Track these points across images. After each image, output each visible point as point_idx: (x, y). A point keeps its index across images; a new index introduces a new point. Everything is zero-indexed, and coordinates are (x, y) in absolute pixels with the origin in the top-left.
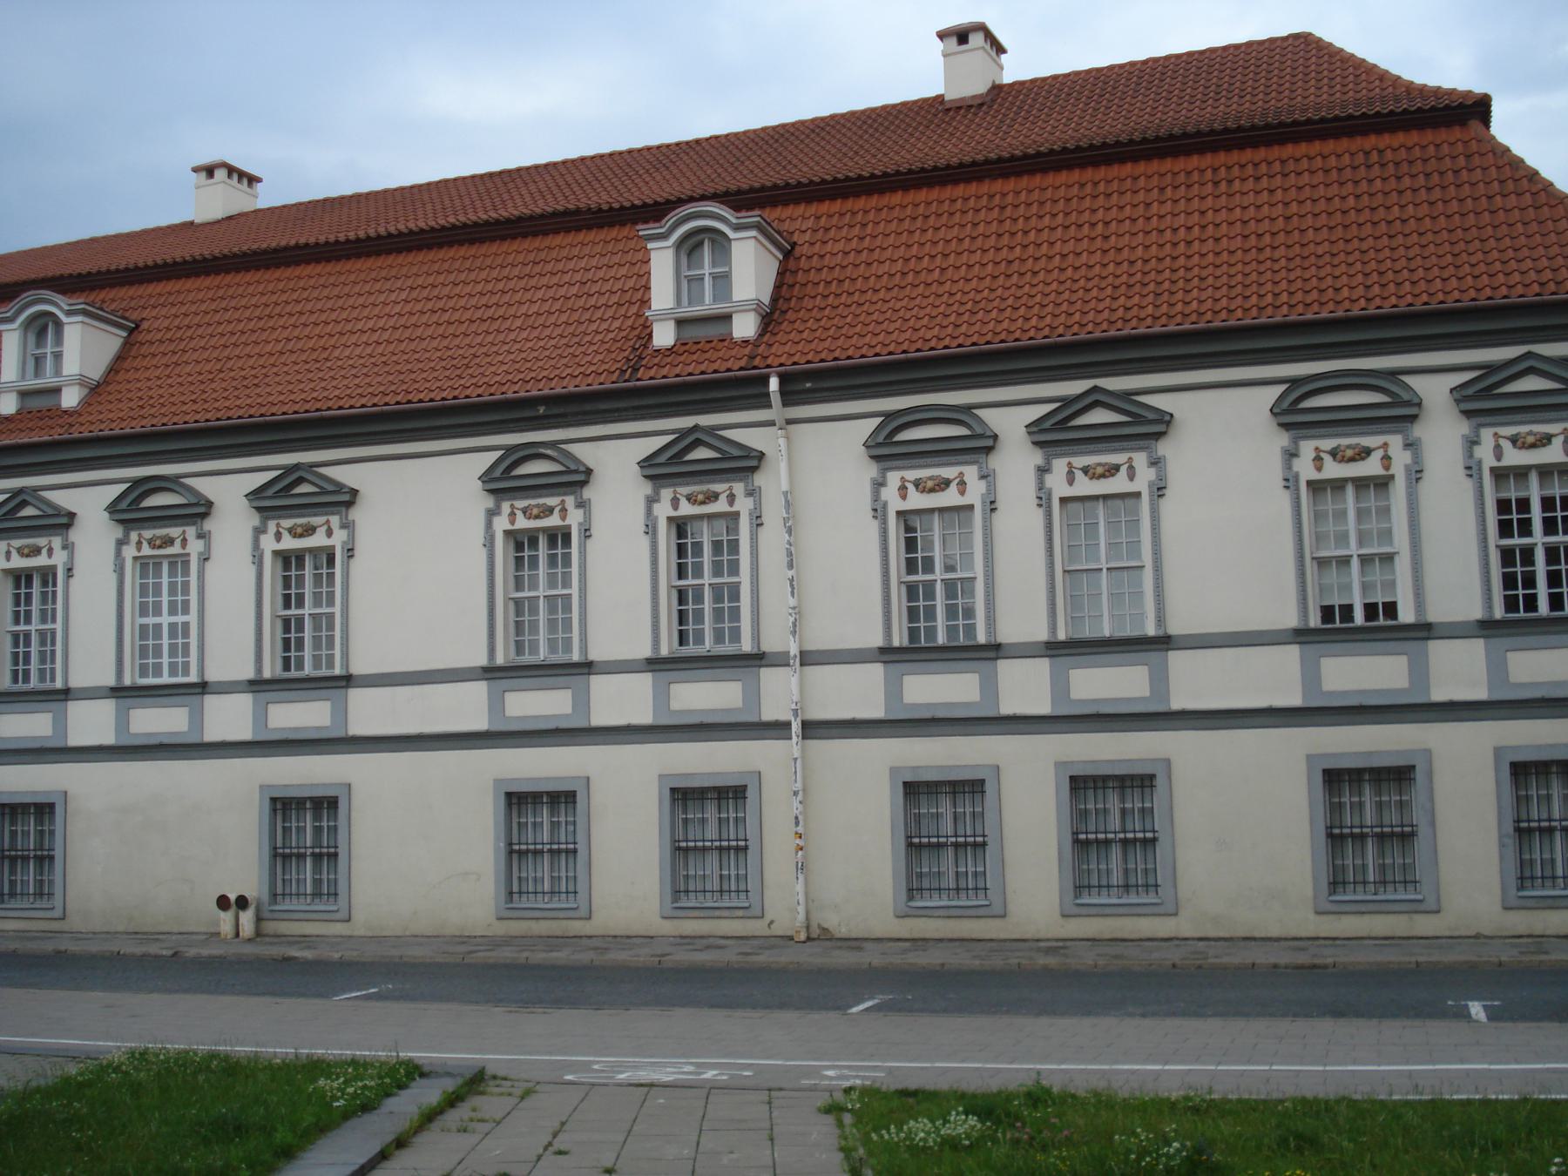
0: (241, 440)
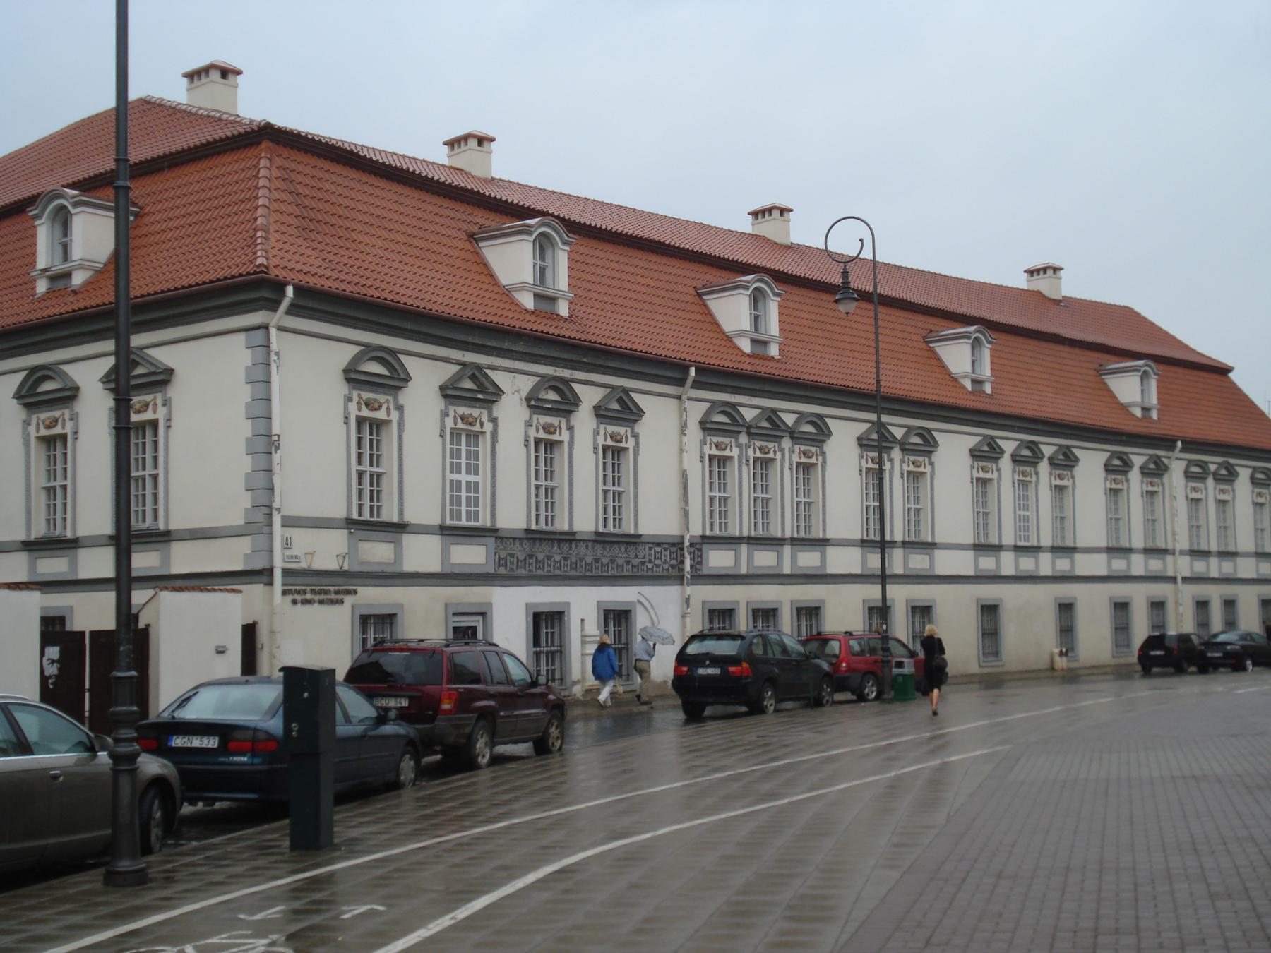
0: (975, 418)
